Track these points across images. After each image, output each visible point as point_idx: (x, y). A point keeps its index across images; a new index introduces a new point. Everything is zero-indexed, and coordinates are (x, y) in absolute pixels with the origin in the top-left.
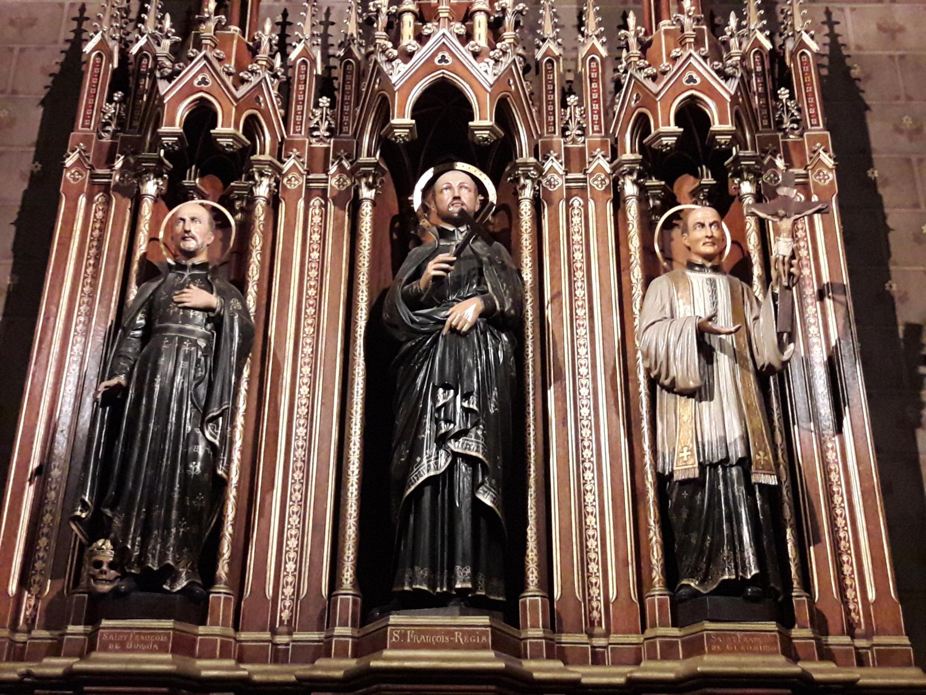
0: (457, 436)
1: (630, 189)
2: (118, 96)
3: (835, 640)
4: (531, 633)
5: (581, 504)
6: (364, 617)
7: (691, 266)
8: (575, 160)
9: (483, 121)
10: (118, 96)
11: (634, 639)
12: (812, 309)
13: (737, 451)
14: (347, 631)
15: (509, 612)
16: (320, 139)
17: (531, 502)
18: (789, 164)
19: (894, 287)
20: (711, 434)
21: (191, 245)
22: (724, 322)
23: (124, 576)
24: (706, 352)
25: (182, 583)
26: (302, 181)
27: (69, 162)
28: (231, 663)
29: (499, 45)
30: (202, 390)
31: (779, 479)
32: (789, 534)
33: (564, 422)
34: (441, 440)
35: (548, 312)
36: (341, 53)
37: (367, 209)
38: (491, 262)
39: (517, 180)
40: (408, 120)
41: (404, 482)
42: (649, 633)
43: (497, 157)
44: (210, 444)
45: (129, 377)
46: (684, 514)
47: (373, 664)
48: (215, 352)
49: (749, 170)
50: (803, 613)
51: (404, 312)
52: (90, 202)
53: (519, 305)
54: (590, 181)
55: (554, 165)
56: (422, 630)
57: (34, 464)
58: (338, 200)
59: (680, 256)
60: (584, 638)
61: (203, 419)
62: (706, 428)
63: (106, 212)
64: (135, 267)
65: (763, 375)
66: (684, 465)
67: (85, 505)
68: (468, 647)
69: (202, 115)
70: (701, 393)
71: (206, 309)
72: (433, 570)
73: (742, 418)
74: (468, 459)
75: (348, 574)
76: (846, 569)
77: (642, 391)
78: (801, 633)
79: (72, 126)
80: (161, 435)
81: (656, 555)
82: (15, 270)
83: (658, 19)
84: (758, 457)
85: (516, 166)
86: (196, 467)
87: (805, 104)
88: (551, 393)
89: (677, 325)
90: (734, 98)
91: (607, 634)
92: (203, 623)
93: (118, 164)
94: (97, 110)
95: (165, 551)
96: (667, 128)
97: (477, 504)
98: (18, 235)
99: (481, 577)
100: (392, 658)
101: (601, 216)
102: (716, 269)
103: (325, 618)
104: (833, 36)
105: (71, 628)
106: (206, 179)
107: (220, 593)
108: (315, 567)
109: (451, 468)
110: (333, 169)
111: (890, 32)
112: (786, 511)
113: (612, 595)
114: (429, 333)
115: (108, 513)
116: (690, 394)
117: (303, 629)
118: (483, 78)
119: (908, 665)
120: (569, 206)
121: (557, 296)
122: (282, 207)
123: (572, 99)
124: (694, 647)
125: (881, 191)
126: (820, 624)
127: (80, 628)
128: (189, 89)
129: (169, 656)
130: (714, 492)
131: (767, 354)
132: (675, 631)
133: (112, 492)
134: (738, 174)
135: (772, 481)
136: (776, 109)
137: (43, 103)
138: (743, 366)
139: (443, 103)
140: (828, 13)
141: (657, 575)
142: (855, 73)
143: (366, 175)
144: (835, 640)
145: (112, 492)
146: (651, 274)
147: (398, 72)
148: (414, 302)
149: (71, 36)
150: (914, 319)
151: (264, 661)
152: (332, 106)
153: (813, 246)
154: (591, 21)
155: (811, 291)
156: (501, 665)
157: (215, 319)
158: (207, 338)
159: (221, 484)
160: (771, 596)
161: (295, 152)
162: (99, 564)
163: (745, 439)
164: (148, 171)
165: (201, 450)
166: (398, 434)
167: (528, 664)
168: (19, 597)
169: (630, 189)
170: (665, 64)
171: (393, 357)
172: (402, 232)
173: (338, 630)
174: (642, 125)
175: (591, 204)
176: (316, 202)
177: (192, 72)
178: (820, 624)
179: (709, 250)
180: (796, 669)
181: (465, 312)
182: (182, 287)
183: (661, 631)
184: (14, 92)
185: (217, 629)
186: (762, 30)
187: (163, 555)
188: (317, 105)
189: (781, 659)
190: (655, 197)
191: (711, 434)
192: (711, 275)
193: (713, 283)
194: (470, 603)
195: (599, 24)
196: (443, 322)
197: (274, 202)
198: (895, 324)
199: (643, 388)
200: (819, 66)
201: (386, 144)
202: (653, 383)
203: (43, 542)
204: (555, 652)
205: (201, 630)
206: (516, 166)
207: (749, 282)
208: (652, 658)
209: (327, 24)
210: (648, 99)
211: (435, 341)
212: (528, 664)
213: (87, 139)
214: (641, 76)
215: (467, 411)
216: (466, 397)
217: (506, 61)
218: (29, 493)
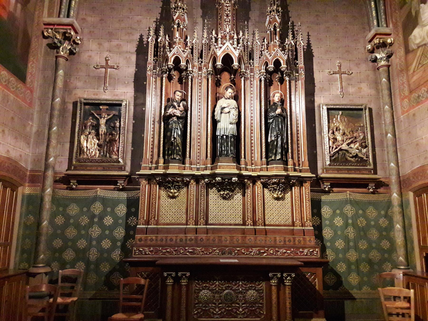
14: (210, 165)
27: (148, 70)
29: (239, 45)
40: (220, 63)
69: (177, 61)
83: (271, 42)
96: (271, 66)
100: (218, 171)
106: (404, 277)
128: (174, 54)
167: (242, 172)
177: (174, 51)
200: (304, 49)
201: (214, 67)
212: (242, 172)
214: (267, 54)
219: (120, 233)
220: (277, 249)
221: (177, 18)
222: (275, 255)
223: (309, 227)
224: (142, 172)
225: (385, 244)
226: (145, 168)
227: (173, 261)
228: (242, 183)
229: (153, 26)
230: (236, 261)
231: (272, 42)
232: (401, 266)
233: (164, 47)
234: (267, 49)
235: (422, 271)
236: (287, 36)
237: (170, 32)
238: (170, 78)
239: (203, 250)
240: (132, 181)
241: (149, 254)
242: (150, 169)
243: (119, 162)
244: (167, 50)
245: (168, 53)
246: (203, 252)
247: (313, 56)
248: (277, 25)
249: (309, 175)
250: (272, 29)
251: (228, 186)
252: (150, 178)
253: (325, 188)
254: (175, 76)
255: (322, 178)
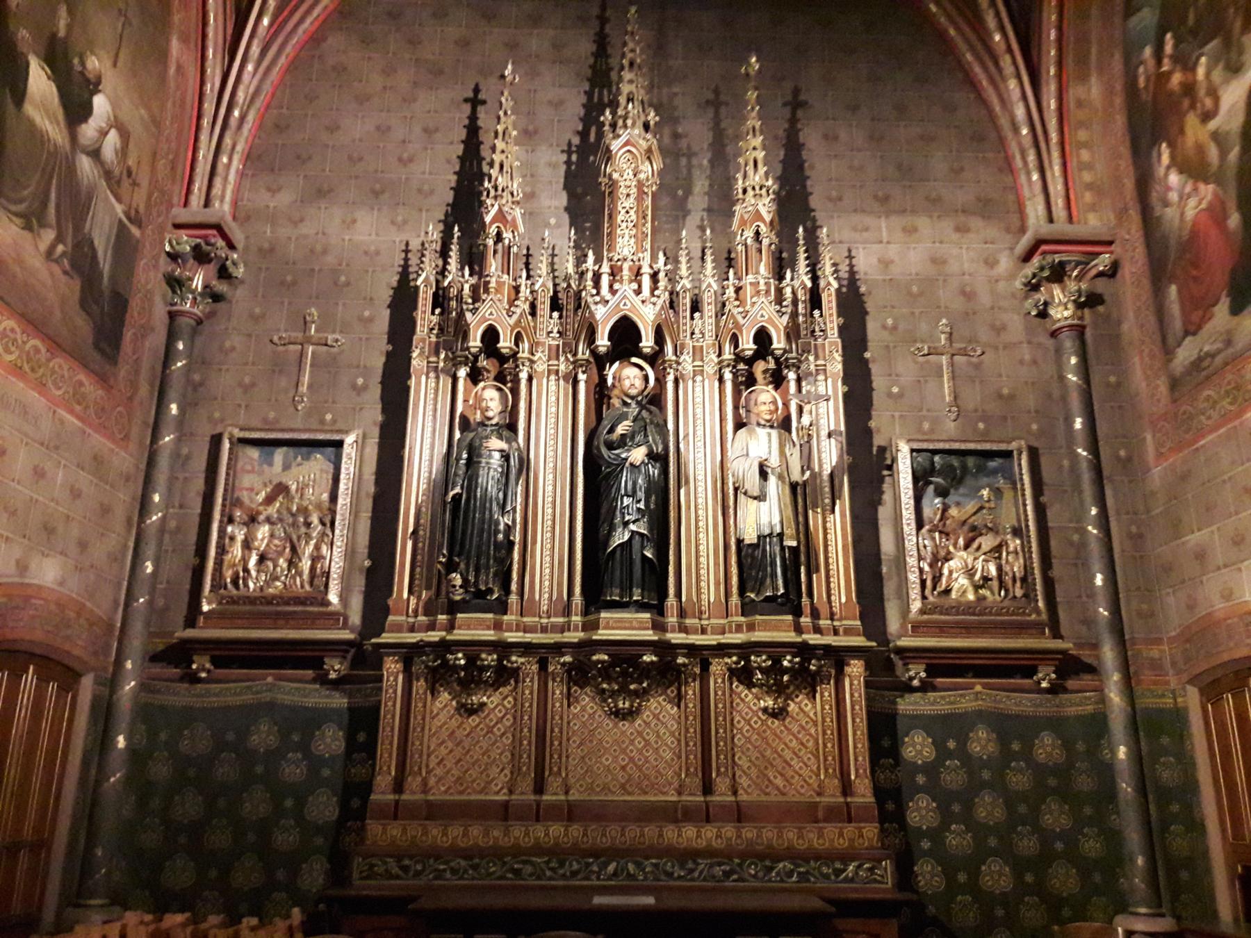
0: (634, 522)
1: (728, 376)
2: (438, 311)
3: (824, 623)
4: (671, 619)
5: (697, 551)
6: (586, 613)
7: (759, 424)
8: (698, 353)
9: (647, 343)
10: (438, 311)
11: (722, 621)
12: (825, 443)
13: (778, 530)
15: (659, 610)
16: (554, 338)
17: (671, 552)
18: (817, 358)
19: (873, 424)
20: (765, 520)
21: (490, 414)
22: (774, 461)
23: (467, 592)
24: (763, 474)
25: (495, 596)
26: (545, 366)
27: (414, 355)
28: (521, 634)
30: (501, 495)
31: (799, 542)
32: (803, 569)
33: (688, 508)
34: (626, 524)
35: (681, 446)
36: (565, 285)
37: (582, 387)
38: (652, 423)
39: (665, 369)
41: (606, 544)
42: (730, 619)
43: (654, 359)
44: (506, 525)
45: (462, 488)
46: (749, 561)
47: (595, 637)
48: (506, 474)
49: (793, 365)
50: (807, 609)
51: (604, 450)
52: (427, 378)
53: (666, 448)
54: (705, 367)
55: (686, 358)
56: (620, 620)
57: (411, 530)
58: (566, 378)
59: (753, 419)
60: (697, 621)
61: (503, 511)
62: (762, 516)
63: (437, 383)
64: (457, 420)
65: (794, 487)
66: (750, 537)
67: (444, 556)
68: (640, 629)
69: (491, 335)
70: (761, 498)
71: (501, 451)
72: (622, 589)
73: (781, 512)
74: (638, 533)
75: (578, 590)
76: (832, 585)
77: (729, 497)
78: (805, 620)
79: (413, 332)
80: (483, 521)
81: (735, 580)
82: (384, 411)
84: (788, 532)
85: (664, 362)
86: (501, 536)
87: (830, 319)
88: (682, 491)
89: (749, 461)
90: (786, 328)
91: (709, 618)
92: (505, 613)
93: (442, 356)
94: (426, 319)
95: (488, 581)
96: (748, 345)
97: (644, 557)
98: (383, 390)
99: (646, 593)
100: (602, 634)
101: (712, 388)
102: (772, 427)
103: (567, 611)
104: (851, 266)
105: (440, 617)
107: (513, 598)
108: (560, 584)
109: (630, 539)
110: (562, 359)
111: (885, 263)
112: (801, 558)
113: (712, 600)
114: (618, 465)
115: (456, 559)
116: (755, 498)
117: (556, 616)
118: (646, 316)
119: (859, 635)
120: (694, 381)
121: (686, 436)
122: (534, 382)
123: (697, 315)
124: (751, 627)
125: (871, 366)
126: (815, 614)
127: (444, 617)
129: (492, 632)
130: (764, 550)
131: (796, 476)
132: (743, 619)
133: (457, 548)
134: (787, 367)
135: (794, 544)
136: (812, 323)
137: (389, 306)
138: (783, 482)
139: (625, 333)
140: (850, 251)
141: (735, 590)
142: (863, 289)
143: (581, 366)
144: (824, 623)
145: (457, 548)
146: (739, 425)
147: (600, 312)
148: (611, 446)
149: (402, 262)
150: (883, 443)
151: (536, 632)
152: (560, 317)
153: (826, 413)
154: (709, 258)
155: (824, 433)
156: (656, 638)
157: (506, 457)
158: (502, 466)
159: (512, 544)
160: (790, 603)
161: (540, 349)
162: (454, 586)
163: (782, 523)
164: (460, 363)
165: (502, 527)
166: (602, 517)
168: (408, 599)
169: (728, 376)
170: (748, 308)
171: (599, 478)
172: (601, 393)
173: (574, 618)
174: (735, 340)
175: (706, 382)
176: (553, 377)
178: (815, 614)
179: (768, 417)
180: (799, 640)
181: (638, 455)
182: (487, 437)
183: (735, 619)
184: (371, 299)
185: (513, 617)
186: (807, 273)
187: (487, 584)
188: (551, 317)
189: (793, 634)
190: (742, 375)
191: (765, 520)
192: (768, 430)
193: (769, 435)
194: (642, 606)
195: (714, 268)
196: (626, 459)
197: (530, 379)
198: (871, 445)
199: (731, 491)
201: (594, 353)
202: (736, 489)
203: (418, 570)
204: (683, 629)
205: (505, 617)
206: (664, 362)
207: (790, 431)
208: (731, 632)
209: (553, 255)
210: (737, 325)
211: (622, 470)
212: (669, 636)
213: (423, 340)
214: (735, 311)
215: (639, 509)
216: (639, 502)
217: (660, 302)
218: (410, 544)
219: (324, 807)
220: (768, 863)
221: (492, 222)
222: (762, 880)
223: (864, 793)
224: (387, 638)
225: (1091, 846)
226: (398, 628)
227: (468, 902)
228: (666, 668)
229: (434, 233)
230: (650, 900)
231: (750, 276)
232: (1141, 906)
233: (460, 298)
234: (737, 299)
235: (1236, 920)
236: (793, 264)
237: (474, 260)
238: (475, 376)
239: (552, 865)
240: (364, 657)
241: (398, 877)
242: (412, 629)
243: (328, 603)
244: (465, 307)
245: (468, 315)
246: (552, 869)
247: (867, 313)
248: (764, 229)
249: (860, 641)
250: (749, 241)
251: (627, 675)
252: (409, 654)
253: (911, 679)
254: (488, 371)
255: (900, 651)
